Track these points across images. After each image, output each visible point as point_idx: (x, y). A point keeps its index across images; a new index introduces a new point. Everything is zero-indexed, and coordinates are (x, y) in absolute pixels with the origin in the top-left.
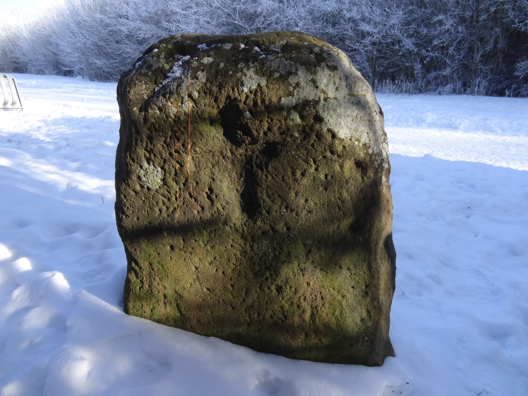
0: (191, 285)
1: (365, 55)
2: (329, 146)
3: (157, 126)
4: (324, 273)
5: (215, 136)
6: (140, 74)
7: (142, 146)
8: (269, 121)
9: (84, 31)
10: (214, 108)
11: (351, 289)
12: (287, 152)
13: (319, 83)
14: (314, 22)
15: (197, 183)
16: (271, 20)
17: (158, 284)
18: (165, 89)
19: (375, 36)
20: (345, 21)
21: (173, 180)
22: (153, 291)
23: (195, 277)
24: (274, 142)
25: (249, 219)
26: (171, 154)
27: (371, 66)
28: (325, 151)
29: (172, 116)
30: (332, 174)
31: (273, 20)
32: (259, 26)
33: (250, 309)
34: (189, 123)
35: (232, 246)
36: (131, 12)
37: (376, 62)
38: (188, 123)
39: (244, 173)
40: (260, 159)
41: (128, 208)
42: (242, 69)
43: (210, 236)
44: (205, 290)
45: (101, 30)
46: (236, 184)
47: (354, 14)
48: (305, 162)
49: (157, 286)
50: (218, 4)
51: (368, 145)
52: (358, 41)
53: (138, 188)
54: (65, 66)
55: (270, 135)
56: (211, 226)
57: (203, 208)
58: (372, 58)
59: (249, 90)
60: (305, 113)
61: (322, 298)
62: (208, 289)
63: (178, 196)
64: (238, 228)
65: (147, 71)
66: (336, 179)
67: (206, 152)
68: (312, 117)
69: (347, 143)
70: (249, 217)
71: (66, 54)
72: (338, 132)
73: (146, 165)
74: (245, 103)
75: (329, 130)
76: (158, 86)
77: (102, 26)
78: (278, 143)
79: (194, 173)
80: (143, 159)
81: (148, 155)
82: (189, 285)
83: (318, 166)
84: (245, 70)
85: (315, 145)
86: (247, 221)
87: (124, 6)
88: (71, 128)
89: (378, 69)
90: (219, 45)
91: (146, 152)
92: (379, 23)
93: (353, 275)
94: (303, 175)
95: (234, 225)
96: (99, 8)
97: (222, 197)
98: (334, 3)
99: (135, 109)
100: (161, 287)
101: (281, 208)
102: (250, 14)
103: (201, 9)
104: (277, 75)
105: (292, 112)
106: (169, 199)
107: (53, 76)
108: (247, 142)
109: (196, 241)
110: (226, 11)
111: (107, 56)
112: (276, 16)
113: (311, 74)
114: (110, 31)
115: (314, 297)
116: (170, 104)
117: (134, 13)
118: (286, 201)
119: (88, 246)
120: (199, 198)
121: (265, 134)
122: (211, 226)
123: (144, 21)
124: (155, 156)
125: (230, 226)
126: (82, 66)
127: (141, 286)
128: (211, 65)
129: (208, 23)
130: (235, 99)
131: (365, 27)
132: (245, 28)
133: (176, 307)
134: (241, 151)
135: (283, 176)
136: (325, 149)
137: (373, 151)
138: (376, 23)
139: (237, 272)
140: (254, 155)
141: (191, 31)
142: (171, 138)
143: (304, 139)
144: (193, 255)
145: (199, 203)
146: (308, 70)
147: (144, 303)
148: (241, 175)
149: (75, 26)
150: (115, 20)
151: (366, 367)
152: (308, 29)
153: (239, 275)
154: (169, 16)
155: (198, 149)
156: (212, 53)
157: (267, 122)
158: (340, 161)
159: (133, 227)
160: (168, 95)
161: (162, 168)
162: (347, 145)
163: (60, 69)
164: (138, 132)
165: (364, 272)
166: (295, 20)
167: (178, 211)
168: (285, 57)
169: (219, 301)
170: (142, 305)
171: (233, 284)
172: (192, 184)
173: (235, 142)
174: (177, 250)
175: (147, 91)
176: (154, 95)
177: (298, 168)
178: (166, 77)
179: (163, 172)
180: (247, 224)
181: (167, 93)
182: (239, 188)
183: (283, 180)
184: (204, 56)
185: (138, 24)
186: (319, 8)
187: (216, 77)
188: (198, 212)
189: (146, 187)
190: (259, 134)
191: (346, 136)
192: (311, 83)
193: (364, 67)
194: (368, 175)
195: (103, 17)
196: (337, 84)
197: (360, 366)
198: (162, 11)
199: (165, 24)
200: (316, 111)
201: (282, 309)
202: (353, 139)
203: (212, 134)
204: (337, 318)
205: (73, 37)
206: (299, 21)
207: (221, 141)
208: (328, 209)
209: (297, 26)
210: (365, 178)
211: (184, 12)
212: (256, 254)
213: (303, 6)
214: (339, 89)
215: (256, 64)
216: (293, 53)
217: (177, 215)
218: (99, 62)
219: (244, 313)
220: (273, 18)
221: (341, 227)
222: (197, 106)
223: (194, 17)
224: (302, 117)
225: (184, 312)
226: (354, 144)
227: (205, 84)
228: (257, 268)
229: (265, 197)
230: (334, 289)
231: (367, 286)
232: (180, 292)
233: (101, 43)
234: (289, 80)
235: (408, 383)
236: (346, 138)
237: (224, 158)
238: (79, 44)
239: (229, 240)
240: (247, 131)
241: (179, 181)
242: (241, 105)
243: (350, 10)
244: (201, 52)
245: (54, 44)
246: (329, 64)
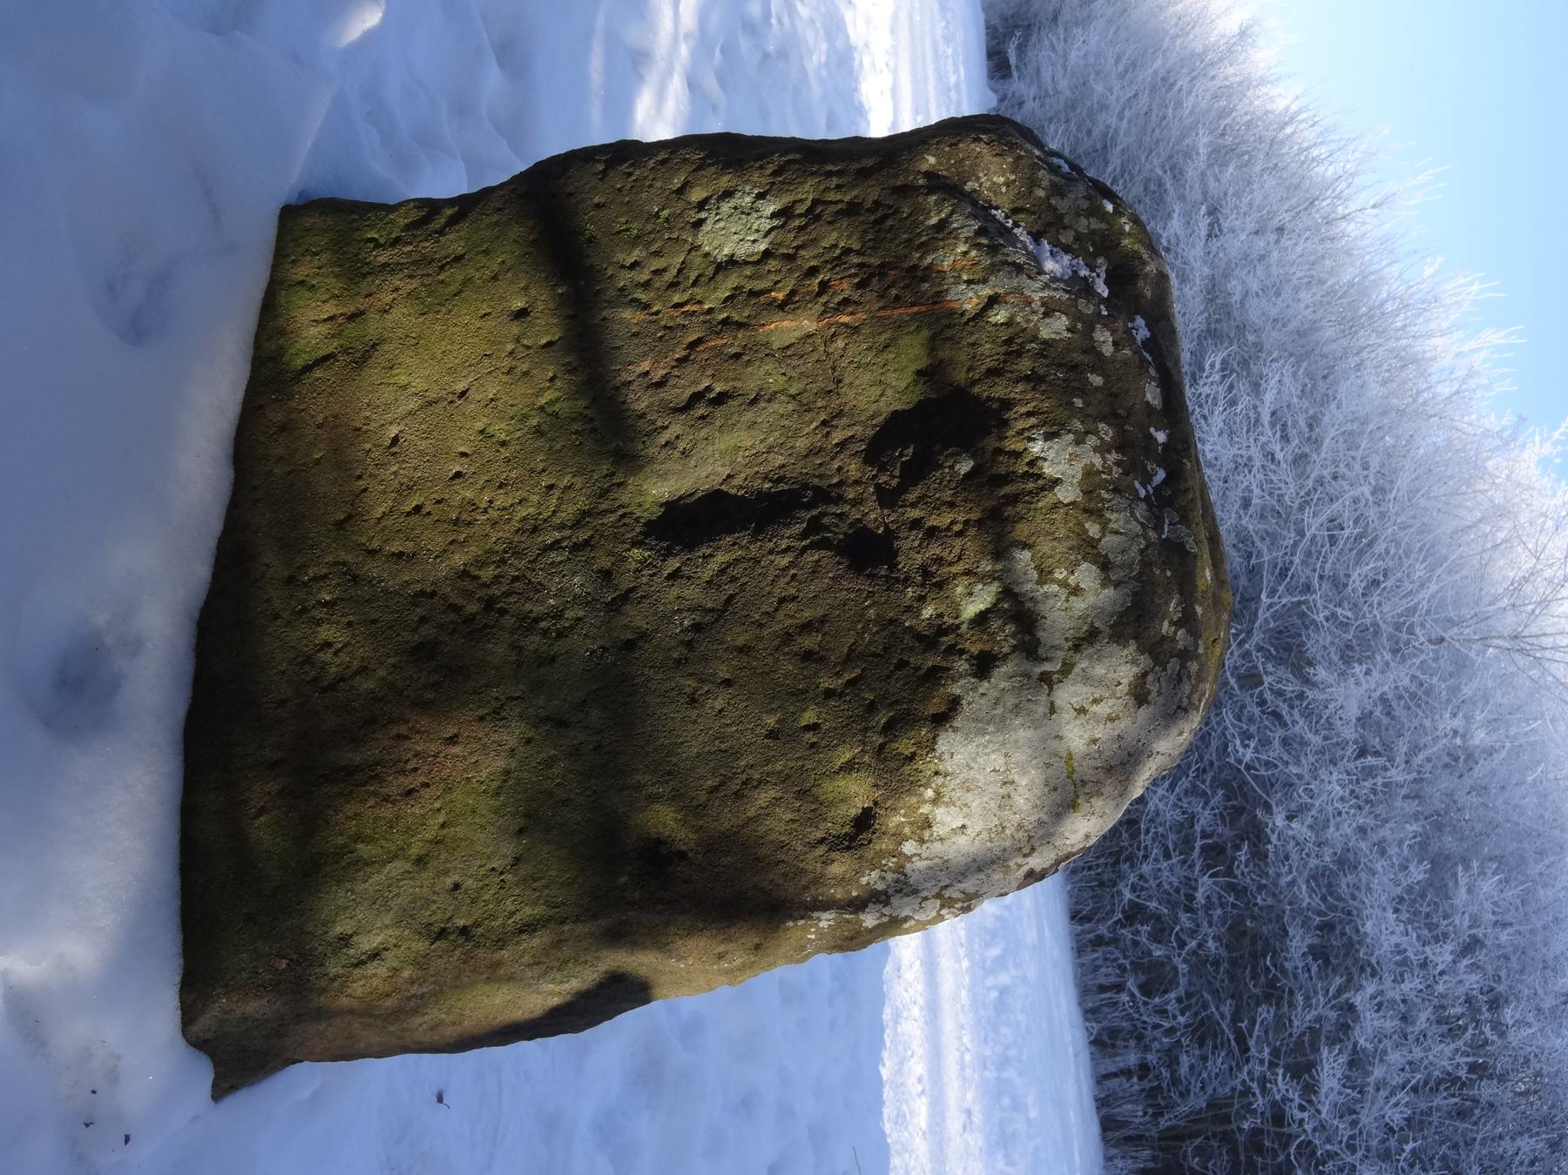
0: (405, 387)
1: (1233, 1089)
2: (908, 712)
3: (889, 222)
4: (495, 784)
5: (881, 385)
6: (1034, 167)
7: (827, 190)
8: (956, 528)
9: (1144, 100)
10: (969, 370)
11: (449, 881)
12: (870, 594)
13: (1091, 650)
14: (1314, 877)
15: (737, 356)
16: (1295, 722)
17: (396, 290)
18: (1001, 235)
19: (1306, 1115)
20: (1340, 991)
21: (735, 289)
22: (370, 279)
23: (432, 395)
24: (895, 553)
25: (645, 525)
26: (813, 271)
27: (1196, 1117)
28: (892, 704)
29: (929, 260)
30: (823, 743)
31: (1297, 729)
32: (1267, 680)
33: (345, 574)
34: (916, 309)
35: (551, 487)
36: (1234, 245)
37: (1215, 1135)
38: (913, 305)
39: (786, 487)
40: (837, 526)
41: (630, 174)
42: (1096, 433)
43: (573, 419)
44: (393, 431)
45: (1159, 155)
46: (749, 471)
47: (1370, 1025)
48: (848, 655)
49: (388, 287)
50: (1313, 530)
51: (926, 834)
52: (1275, 1053)
53: (696, 195)
54: (1021, 49)
55: (915, 538)
56: (605, 427)
57: (660, 385)
58: (1227, 1119)
59: (1038, 458)
60: (995, 624)
61: (409, 793)
62: (395, 440)
63: (686, 308)
64: (612, 495)
65: (1045, 183)
66: (808, 758)
67: (834, 369)
68: (987, 647)
69: (926, 766)
70: (649, 523)
71: (1061, 52)
72: (955, 730)
73: (770, 208)
74: (999, 451)
75: (955, 703)
76: (1007, 217)
77: (1170, 157)
78: (893, 566)
79: (767, 344)
80: (786, 199)
81: (801, 209)
82: (403, 379)
83: (841, 695)
84: (1092, 441)
85: (904, 672)
86: (637, 520)
87: (1248, 220)
88: (824, 73)
89: (1189, 1147)
90: (1152, 372)
91: (808, 203)
92: (1354, 1124)
93: (497, 880)
94: (808, 656)
95: (620, 485)
96: (1229, 140)
97: (703, 433)
98: (1394, 939)
99: (932, 160)
100: (388, 299)
101: (691, 610)
102: (1302, 644)
103: (1285, 472)
104: (1093, 529)
105: (995, 587)
106: (673, 285)
107: (982, 17)
108: (883, 479)
109: (552, 380)
110: (1297, 560)
112: (1309, 736)
113: (1111, 627)
114: (1160, 184)
115: (410, 766)
116: (962, 248)
117: (1233, 253)
118: (717, 621)
119: (463, 109)
120: (690, 370)
121: (916, 524)
122: (605, 427)
123: (1213, 291)
124: (801, 229)
125: (613, 474)
126: (1030, 105)
127: (382, 241)
128: (1092, 350)
129: (1246, 503)
130: (1005, 424)
131: (1330, 1070)
132: (1250, 632)
133: (321, 353)
134: (854, 469)
135: (794, 599)
136: (897, 702)
137: (909, 858)
138: (1355, 1112)
139: (464, 516)
140: (847, 508)
141: (1208, 447)
142: (861, 265)
143: (919, 637)
144: (505, 378)
146: (1121, 615)
147: (325, 257)
148: (781, 480)
149: (1156, 72)
150: (1199, 197)
151: (178, 979)
152: (1287, 858)
153: (456, 522)
154: (1244, 367)
155: (840, 343)
156: (1127, 352)
157: (953, 523)
158: (866, 759)
159: (570, 194)
160: (985, 241)
161: (767, 254)
162: (919, 764)
163: (1008, 35)
164: (864, 174)
165: (513, 914)
166: (1308, 807)
167: (640, 316)
168: (1147, 546)
169: (360, 477)
170: (316, 254)
171: (424, 511)
172: (732, 342)
173: (877, 450)
174: (515, 329)
175: (989, 189)
176: (981, 210)
177: (827, 638)
178: (1036, 237)
179: (755, 258)
180: (627, 521)
181: (991, 239)
182: (736, 482)
183: (782, 601)
184: (1113, 332)
185: (1200, 272)
186: (1369, 889)
187: (1060, 365)
188: (646, 374)
189: (703, 215)
190: (913, 505)
191: (946, 757)
192: (1085, 628)
193: (1188, 1091)
194: (833, 855)
195: (1203, 158)
196: (1095, 708)
197: (181, 961)
198: (1255, 344)
199: (1214, 358)
200: (1006, 656)
201: (356, 673)
202: (940, 780)
203: (891, 378)
204: (344, 850)
205: (1121, 68)
206: (1309, 820)
207: (874, 407)
208: (709, 752)
209: (1290, 818)
210: (821, 850)
211: (1266, 418)
212: (534, 561)
213: (1362, 830)
214: (1082, 719)
215: (1117, 472)
216: (1163, 571)
217: (627, 314)
219: (330, 558)
220: (1301, 727)
221: (657, 806)
222: (966, 323)
223: (1255, 452)
224: (981, 619)
225: (307, 379)
226: (926, 786)
227: (1034, 339)
228: (487, 574)
229: (721, 558)
230: (443, 826)
231: (464, 931)
232: (379, 358)
234: (1085, 565)
235: (127, 1139)
236: (940, 759)
237: (824, 423)
238: (1100, 88)
239: (568, 477)
240: (915, 472)
241: (734, 307)
242: (991, 443)
243: (1380, 1005)
244: (1125, 325)
245: (1086, 13)
246: (1150, 678)
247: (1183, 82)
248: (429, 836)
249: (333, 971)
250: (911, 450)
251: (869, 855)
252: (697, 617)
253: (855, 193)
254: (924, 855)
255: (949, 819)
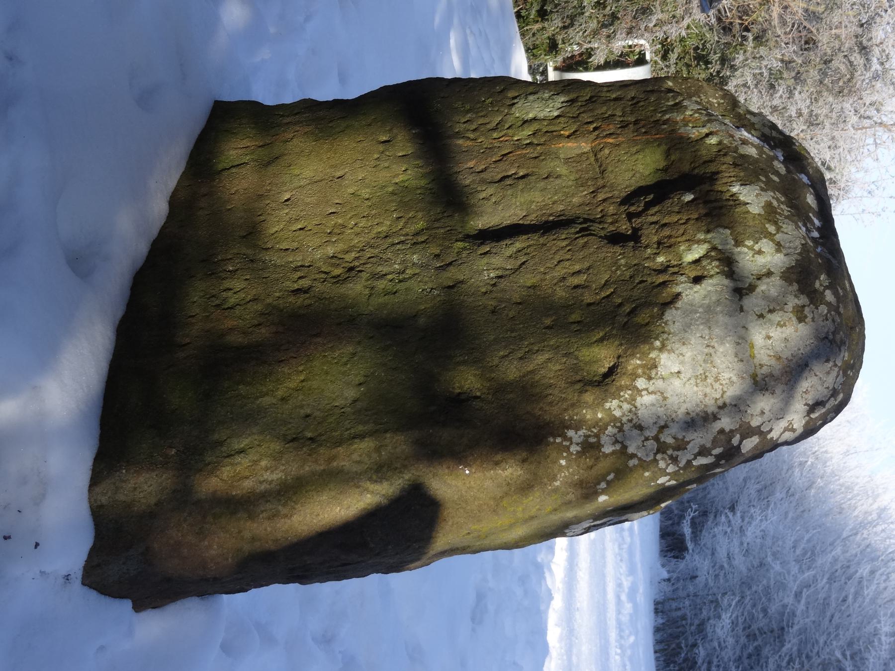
3: (642, 104)
111: (749, 656)
145: (493, 166)
149: (836, 560)
162: (652, 328)
202: (665, 336)
207: (627, 183)
218: (723, 627)
219: (235, 251)
226: (656, 339)
230: (302, 381)
233: (791, 644)
235: (37, 545)
236: (666, 323)
238: (777, 567)
247: (864, 570)
248: (292, 385)
249: (208, 459)
250: (652, 196)
251: (613, 389)
252: (500, 273)
253: (619, 93)
254: (650, 390)
255: (669, 363)
